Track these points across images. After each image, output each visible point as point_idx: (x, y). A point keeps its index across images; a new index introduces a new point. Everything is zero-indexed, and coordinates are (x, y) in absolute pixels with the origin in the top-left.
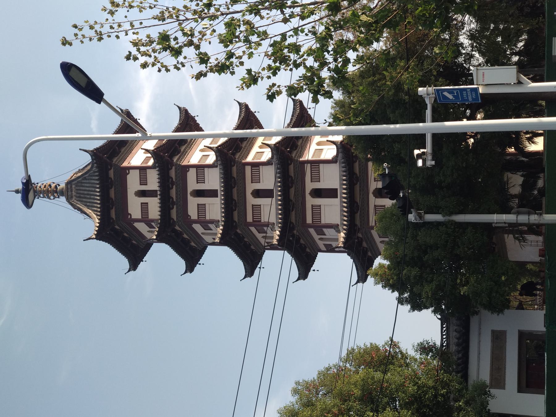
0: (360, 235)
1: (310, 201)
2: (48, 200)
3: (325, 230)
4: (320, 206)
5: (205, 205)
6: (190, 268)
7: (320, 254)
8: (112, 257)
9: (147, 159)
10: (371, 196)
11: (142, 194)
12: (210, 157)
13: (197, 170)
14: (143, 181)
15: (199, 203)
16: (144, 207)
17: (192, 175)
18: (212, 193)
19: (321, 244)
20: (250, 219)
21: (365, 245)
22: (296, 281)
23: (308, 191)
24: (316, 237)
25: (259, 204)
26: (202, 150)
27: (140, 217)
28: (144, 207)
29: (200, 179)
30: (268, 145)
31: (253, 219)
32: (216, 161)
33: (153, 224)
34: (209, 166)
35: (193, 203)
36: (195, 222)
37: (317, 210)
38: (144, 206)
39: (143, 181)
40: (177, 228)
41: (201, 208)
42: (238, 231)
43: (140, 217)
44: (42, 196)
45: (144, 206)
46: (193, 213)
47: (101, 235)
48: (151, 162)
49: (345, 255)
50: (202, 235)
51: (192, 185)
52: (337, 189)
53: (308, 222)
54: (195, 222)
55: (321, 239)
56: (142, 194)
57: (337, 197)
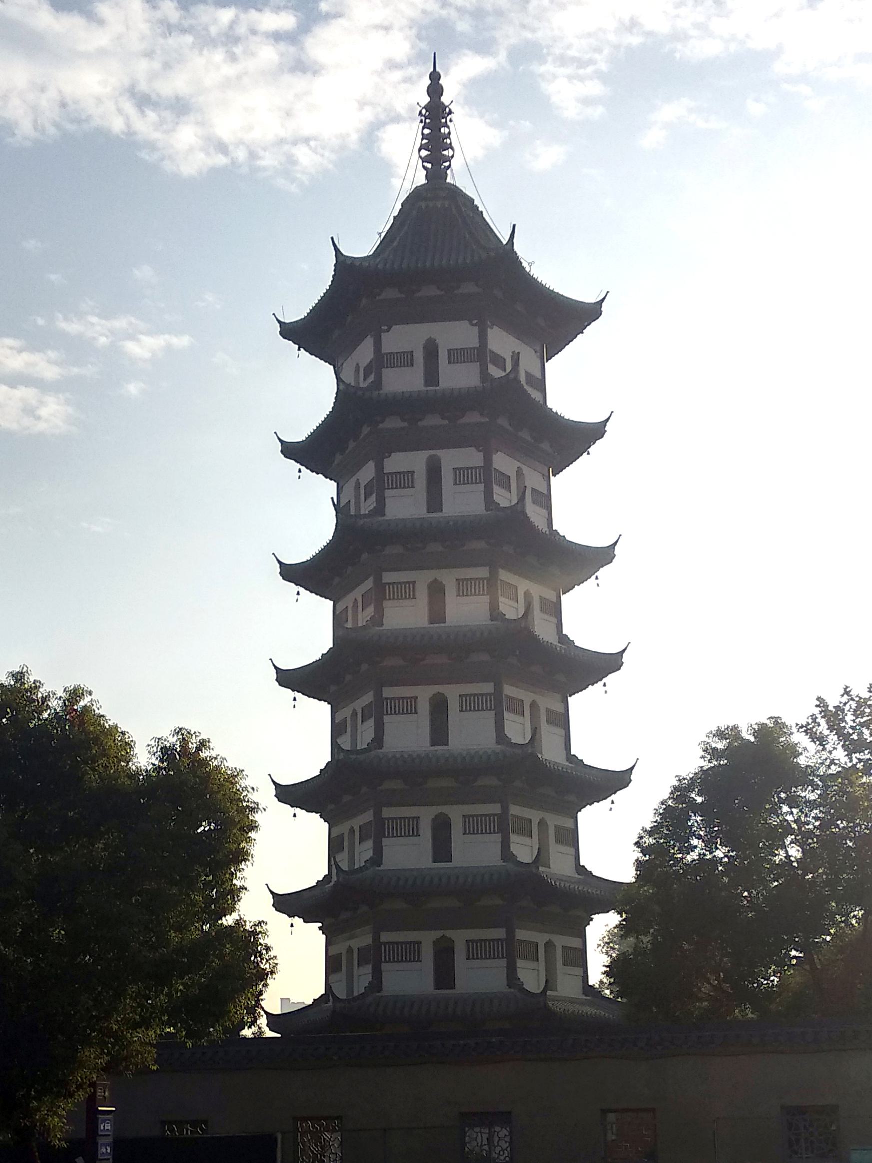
0: (364, 789)
1: (426, 815)
2: (418, 145)
3: (371, 722)
4: (414, 598)
5: (416, 713)
6: (290, 450)
7: (329, 604)
8: (305, 288)
9: (499, 361)
10: (436, 934)
11: (431, 350)
12: (507, 494)
13: (490, 694)
14: (457, 356)
15: (417, 586)
16: (405, 359)
17: (471, 457)
18: (435, 501)
19: (346, 712)
20: (389, 577)
21: (347, 798)
22: (274, 665)
23: (449, 933)
24: (357, 594)
25: (421, 832)
26: (519, 473)
27: (385, 349)
28: (405, 359)
29: (462, 476)
30: (522, 499)
31: (388, 819)
32: (493, 380)
33: (372, 378)
34: (512, 970)
35: (414, 462)
36: (379, 468)
37: (409, 707)
38: (406, 359)
39: (457, 356)
40: (366, 430)
41: (405, 479)
42: (365, 556)
43: (385, 349)
44: (427, 131)
45: (406, 359)
46: (397, 462)
47: (345, 267)
48: (495, 372)
49: (321, 871)
50: (354, 479)
51: (452, 459)
52: (453, 987)
53: (385, 810)
54: (379, 468)
55: (354, 713)
56: (431, 350)
57: (437, 987)
